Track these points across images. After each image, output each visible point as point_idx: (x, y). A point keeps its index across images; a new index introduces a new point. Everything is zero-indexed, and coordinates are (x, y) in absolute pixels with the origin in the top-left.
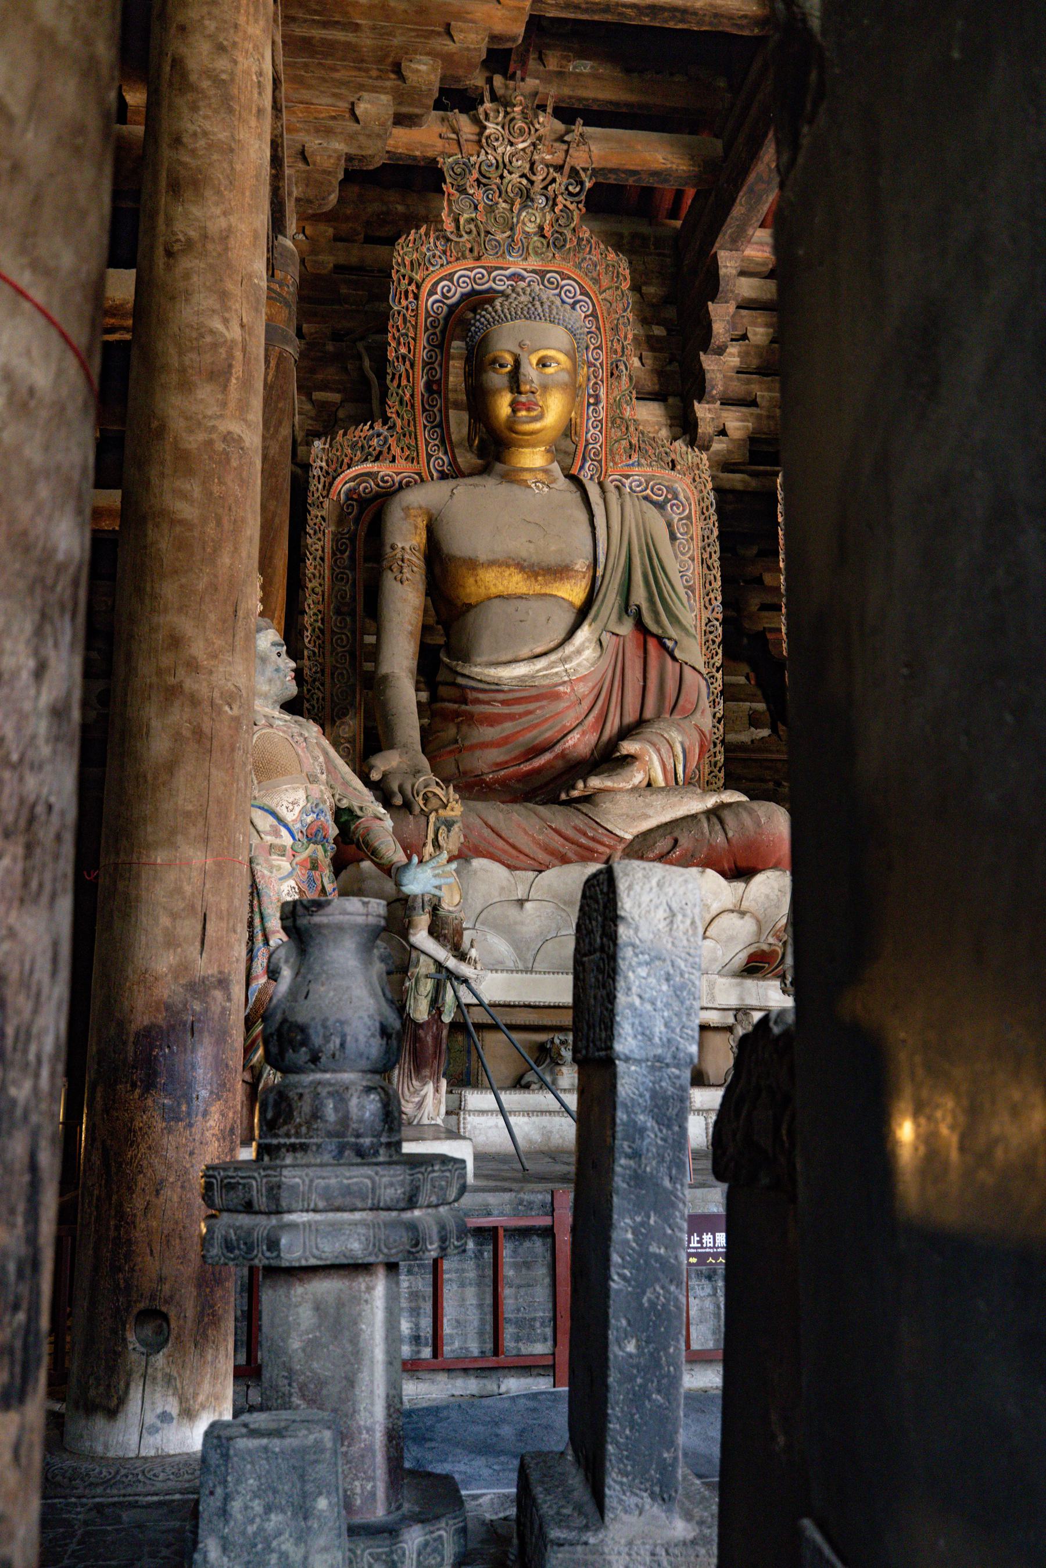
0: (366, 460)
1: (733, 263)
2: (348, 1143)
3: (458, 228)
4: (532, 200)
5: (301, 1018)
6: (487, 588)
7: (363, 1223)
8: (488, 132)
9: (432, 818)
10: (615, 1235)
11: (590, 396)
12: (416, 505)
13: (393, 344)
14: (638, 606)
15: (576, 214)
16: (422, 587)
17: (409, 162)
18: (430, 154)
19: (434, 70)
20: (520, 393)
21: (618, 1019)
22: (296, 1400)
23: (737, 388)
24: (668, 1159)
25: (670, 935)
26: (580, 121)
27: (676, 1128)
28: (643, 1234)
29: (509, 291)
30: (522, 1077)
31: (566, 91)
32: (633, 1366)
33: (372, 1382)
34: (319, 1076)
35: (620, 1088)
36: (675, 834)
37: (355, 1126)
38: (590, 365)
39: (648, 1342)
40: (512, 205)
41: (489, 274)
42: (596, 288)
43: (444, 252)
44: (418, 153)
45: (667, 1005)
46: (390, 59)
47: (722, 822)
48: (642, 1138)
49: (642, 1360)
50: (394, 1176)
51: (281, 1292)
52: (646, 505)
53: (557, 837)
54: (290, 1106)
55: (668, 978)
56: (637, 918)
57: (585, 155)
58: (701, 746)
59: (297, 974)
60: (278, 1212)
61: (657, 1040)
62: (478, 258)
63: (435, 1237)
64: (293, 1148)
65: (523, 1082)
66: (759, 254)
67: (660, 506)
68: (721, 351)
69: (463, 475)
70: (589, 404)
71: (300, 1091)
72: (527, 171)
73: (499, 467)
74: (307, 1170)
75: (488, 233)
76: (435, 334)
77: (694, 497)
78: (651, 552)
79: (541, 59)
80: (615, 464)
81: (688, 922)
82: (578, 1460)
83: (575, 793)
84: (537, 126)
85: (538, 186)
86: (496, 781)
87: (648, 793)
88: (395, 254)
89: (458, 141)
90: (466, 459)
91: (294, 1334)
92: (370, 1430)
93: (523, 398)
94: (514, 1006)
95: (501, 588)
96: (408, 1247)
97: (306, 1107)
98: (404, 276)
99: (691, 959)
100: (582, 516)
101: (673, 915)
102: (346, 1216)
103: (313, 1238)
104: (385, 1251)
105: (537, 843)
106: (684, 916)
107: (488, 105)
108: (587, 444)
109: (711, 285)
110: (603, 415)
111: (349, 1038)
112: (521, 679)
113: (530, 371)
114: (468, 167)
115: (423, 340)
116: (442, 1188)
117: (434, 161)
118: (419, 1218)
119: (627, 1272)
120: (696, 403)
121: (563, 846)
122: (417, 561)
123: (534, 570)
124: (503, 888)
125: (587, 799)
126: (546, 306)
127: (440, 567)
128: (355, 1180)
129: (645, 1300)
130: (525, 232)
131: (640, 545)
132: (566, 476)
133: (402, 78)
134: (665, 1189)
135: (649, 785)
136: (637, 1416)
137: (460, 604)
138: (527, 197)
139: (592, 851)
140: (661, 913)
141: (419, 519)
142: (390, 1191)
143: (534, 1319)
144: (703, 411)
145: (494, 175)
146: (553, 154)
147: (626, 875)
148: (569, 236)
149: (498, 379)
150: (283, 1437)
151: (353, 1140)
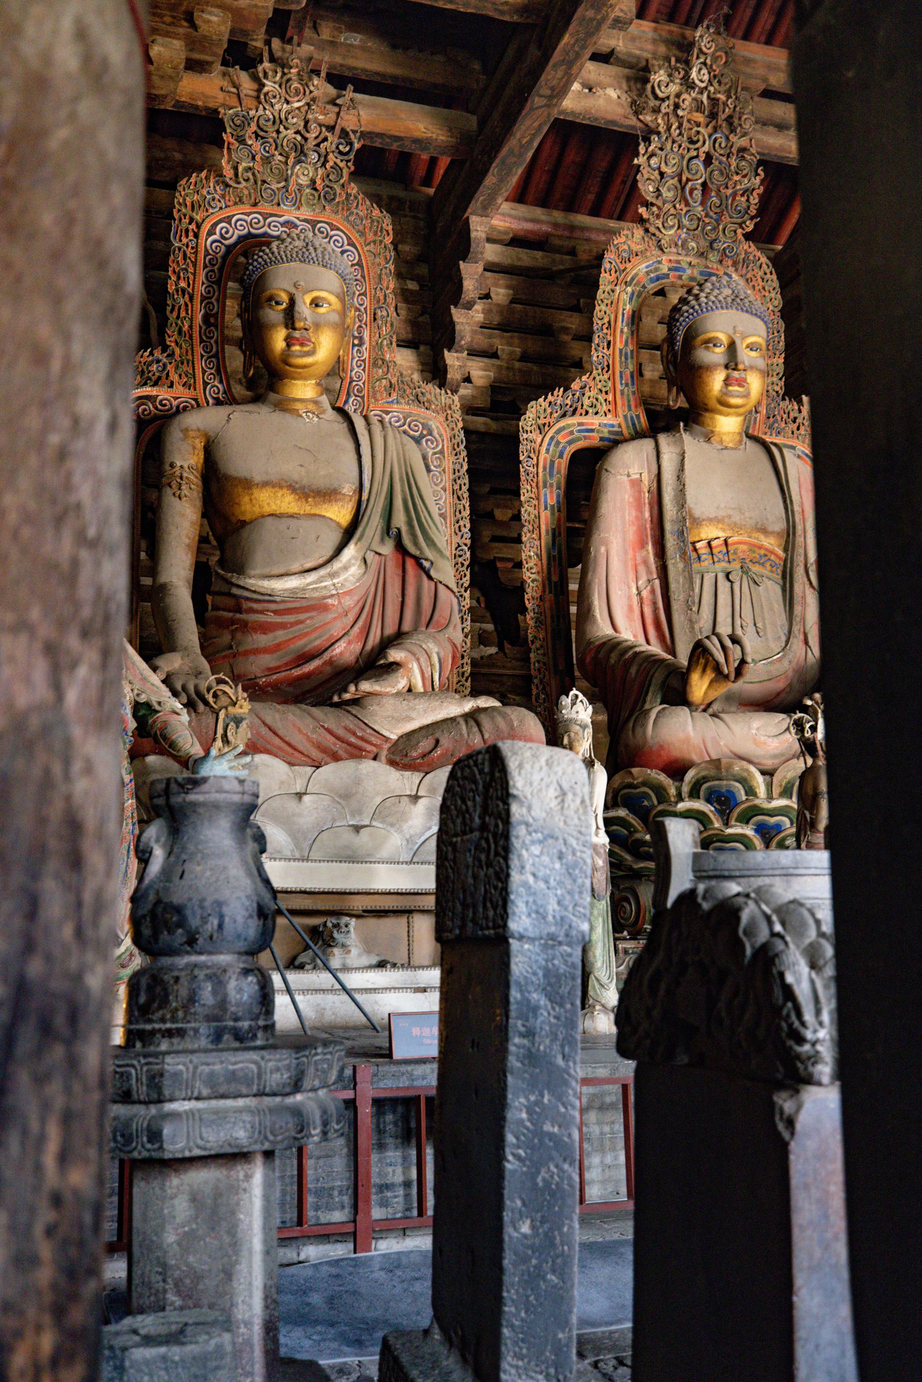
0: (145, 384)
1: (483, 228)
2: (225, 1027)
3: (236, 175)
4: (305, 155)
5: (176, 899)
6: (261, 507)
7: (248, 1110)
8: (266, 89)
9: (222, 714)
10: (511, 1115)
11: (355, 337)
12: (194, 427)
13: (174, 278)
14: (399, 529)
15: (345, 172)
16: (199, 504)
17: (191, 111)
18: (211, 105)
19: (225, 22)
20: (294, 329)
21: (512, 897)
22: (171, 1297)
23: (481, 341)
24: (561, 1037)
25: (562, 814)
26: (350, 87)
27: (568, 1006)
28: (536, 1112)
29: (284, 236)
30: (295, 958)
31: (338, 60)
32: (528, 1247)
33: (250, 1274)
34: (194, 958)
35: (513, 967)
36: (437, 735)
37: (233, 1009)
38: (357, 310)
39: (542, 1222)
40: (287, 158)
41: (265, 219)
42: (362, 240)
43: (223, 196)
44: (200, 103)
45: (560, 883)
46: (183, 8)
47: (478, 725)
48: (536, 1018)
49: (537, 1241)
50: (279, 1060)
51: (155, 1184)
52: (405, 437)
53: (329, 737)
54: (165, 990)
55: (561, 856)
56: (529, 797)
57: (355, 119)
58: (454, 658)
59: (170, 854)
60: (160, 1101)
61: (550, 918)
62: (255, 204)
63: (318, 1122)
64: (169, 1033)
65: (297, 963)
66: (502, 224)
67: (417, 441)
68: (469, 306)
69: (237, 402)
70: (354, 345)
71: (176, 973)
72: (301, 128)
73: (272, 396)
74: (190, 1057)
75: (264, 182)
76: (213, 271)
77: (447, 434)
78: (410, 481)
79: (315, 27)
80: (376, 400)
81: (578, 801)
82: (448, 1340)
83: (347, 696)
84: (312, 88)
85: (311, 143)
86: (269, 685)
87: (411, 697)
88: (177, 194)
89: (238, 96)
90: (239, 390)
91: (169, 1228)
92: (248, 1324)
93: (297, 334)
94: (291, 892)
95: (274, 507)
96: (293, 1134)
97: (183, 991)
98: (185, 215)
99: (582, 838)
100: (350, 445)
101: (564, 794)
102: (229, 1103)
103: (197, 1127)
104: (271, 1138)
105: (309, 740)
106: (575, 794)
107: (266, 65)
108: (352, 381)
109: (463, 246)
110: (366, 355)
111: (227, 919)
112: (293, 591)
113: (304, 309)
114: (247, 120)
115: (201, 276)
116: (324, 1072)
117: (216, 111)
118: (302, 1103)
119: (521, 1152)
120: (446, 352)
121: (335, 744)
122: (194, 478)
123: (305, 492)
124: (282, 783)
125: (355, 702)
126: (319, 252)
127: (218, 488)
128: (240, 1065)
129: (539, 1179)
130: (298, 184)
131: (401, 474)
132: (334, 408)
133: (194, 27)
134: (558, 1067)
135: (410, 690)
136: (532, 1298)
137: (234, 519)
138: (301, 152)
139: (360, 749)
140: (552, 792)
141: (197, 441)
142: (276, 1076)
143: (332, 1188)
144: (452, 359)
145: (271, 129)
146: (325, 114)
147: (515, 754)
148: (338, 191)
149: (274, 315)
150: (183, 1344)
151: (231, 1023)
